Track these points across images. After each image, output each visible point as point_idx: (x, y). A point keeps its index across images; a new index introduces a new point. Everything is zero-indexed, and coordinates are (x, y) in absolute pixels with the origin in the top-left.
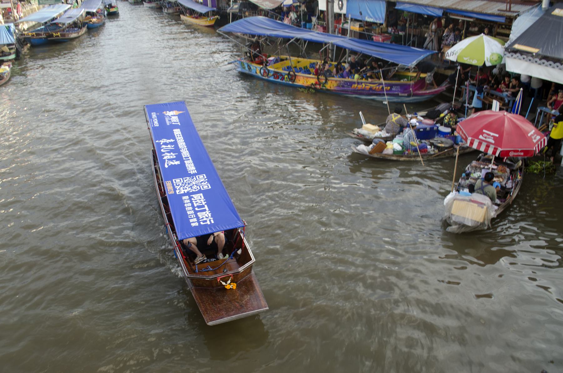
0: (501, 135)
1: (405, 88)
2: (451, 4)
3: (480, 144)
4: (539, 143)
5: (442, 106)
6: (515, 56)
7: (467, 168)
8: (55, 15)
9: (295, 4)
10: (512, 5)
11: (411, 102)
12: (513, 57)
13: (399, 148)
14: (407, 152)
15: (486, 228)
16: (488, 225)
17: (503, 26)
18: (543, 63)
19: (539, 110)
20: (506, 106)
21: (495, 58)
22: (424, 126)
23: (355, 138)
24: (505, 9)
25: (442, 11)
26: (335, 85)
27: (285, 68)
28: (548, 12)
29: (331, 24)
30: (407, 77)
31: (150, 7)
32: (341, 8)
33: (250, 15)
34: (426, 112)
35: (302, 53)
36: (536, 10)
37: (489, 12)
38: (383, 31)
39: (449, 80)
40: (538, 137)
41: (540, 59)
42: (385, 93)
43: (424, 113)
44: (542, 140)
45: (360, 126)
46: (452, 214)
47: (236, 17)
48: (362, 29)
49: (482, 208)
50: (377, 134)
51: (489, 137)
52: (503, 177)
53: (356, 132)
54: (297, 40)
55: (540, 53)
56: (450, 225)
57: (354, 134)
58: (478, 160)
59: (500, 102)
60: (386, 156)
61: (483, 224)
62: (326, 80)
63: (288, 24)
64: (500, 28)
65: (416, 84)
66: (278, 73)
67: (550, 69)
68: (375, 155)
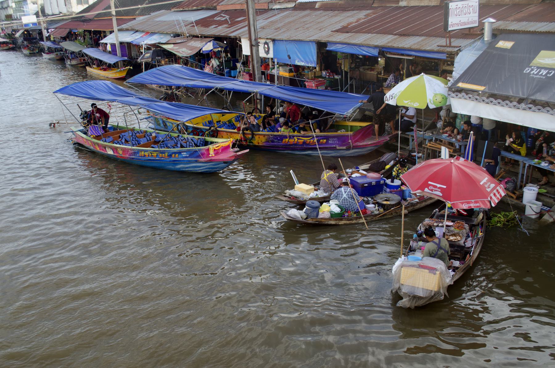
1: (343, 140)
2: (386, 42)
5: (386, 157)
6: (460, 95)
7: (419, 228)
9: (216, 50)
10: (452, 40)
11: (352, 155)
13: (337, 210)
15: (442, 298)
16: (445, 295)
17: (449, 63)
18: (492, 102)
20: (456, 152)
21: (439, 99)
22: (368, 180)
23: (286, 201)
24: (445, 44)
25: (378, 50)
26: (264, 141)
27: (205, 122)
28: (492, 45)
29: (257, 70)
30: (345, 128)
31: (49, 59)
32: (267, 52)
33: (166, 64)
34: (369, 165)
35: (226, 104)
36: (478, 44)
37: (428, 48)
38: (317, 75)
40: (493, 185)
41: (488, 98)
42: (317, 147)
43: (366, 166)
46: (402, 285)
47: (149, 66)
48: (292, 74)
49: (435, 274)
50: (313, 194)
51: (435, 189)
53: (287, 195)
54: (221, 90)
55: (487, 91)
56: (402, 298)
57: (285, 196)
58: (432, 217)
59: (448, 148)
60: (323, 221)
61: (437, 293)
62: (253, 135)
63: (210, 72)
65: (355, 135)
66: (198, 129)
67: (499, 108)
68: (310, 221)
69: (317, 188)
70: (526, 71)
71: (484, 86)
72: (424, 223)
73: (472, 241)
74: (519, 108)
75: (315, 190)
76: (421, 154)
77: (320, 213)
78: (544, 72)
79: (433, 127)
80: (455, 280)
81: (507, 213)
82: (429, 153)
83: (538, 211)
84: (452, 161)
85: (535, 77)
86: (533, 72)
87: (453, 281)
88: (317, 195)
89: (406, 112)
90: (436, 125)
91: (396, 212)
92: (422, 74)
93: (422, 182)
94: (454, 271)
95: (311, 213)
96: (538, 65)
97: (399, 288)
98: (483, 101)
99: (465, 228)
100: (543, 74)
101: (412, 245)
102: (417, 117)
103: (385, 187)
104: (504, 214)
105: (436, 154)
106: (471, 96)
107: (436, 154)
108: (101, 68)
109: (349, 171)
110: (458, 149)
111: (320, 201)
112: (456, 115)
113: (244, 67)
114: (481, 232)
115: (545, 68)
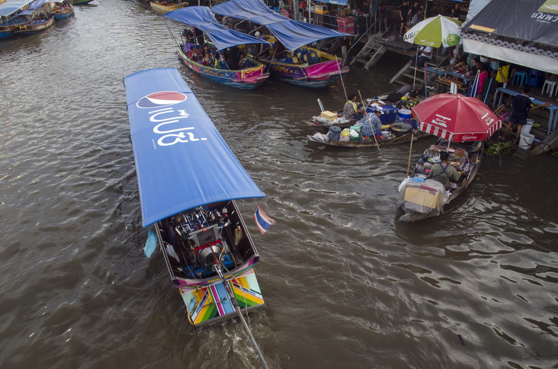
0: (454, 119)
3: (433, 128)
4: (493, 126)
6: (471, 36)
7: (425, 153)
8: (21, 7)
12: (469, 37)
14: (364, 139)
15: (438, 214)
16: (441, 212)
18: (499, 43)
19: (497, 91)
20: (464, 90)
21: (453, 39)
38: (348, 13)
39: (411, 62)
41: (496, 40)
44: (497, 123)
45: (318, 113)
46: (406, 201)
48: (326, 12)
49: (434, 194)
50: (336, 121)
51: (441, 121)
52: (460, 160)
53: (314, 120)
55: (496, 33)
58: (437, 144)
61: (435, 210)
64: (463, 7)
67: (505, 50)
68: (332, 143)
69: (340, 114)
70: (534, 16)
71: (494, 28)
72: (430, 148)
73: (470, 166)
74: (523, 50)
75: (338, 116)
76: (433, 88)
77: (341, 137)
78: (549, 18)
79: (446, 63)
80: (451, 199)
81: (504, 144)
82: (441, 87)
83: (531, 143)
84: (459, 97)
85: (541, 21)
86: (540, 17)
87: (449, 200)
88: (339, 121)
89: (424, 49)
90: (449, 62)
91: (407, 139)
92: (440, 15)
93: (430, 115)
94: (451, 192)
95: (333, 136)
96: (545, 11)
97: (403, 204)
98: (492, 42)
99: (464, 155)
100: (549, 20)
101: (418, 167)
102: (433, 54)
103: (398, 116)
104: (501, 144)
105: (445, 89)
106: (481, 37)
107: (445, 89)
108: (163, 3)
109: (369, 100)
110: (466, 84)
111: (342, 126)
112: (467, 54)
113: (285, 4)
114: (478, 159)
115: (551, 14)
